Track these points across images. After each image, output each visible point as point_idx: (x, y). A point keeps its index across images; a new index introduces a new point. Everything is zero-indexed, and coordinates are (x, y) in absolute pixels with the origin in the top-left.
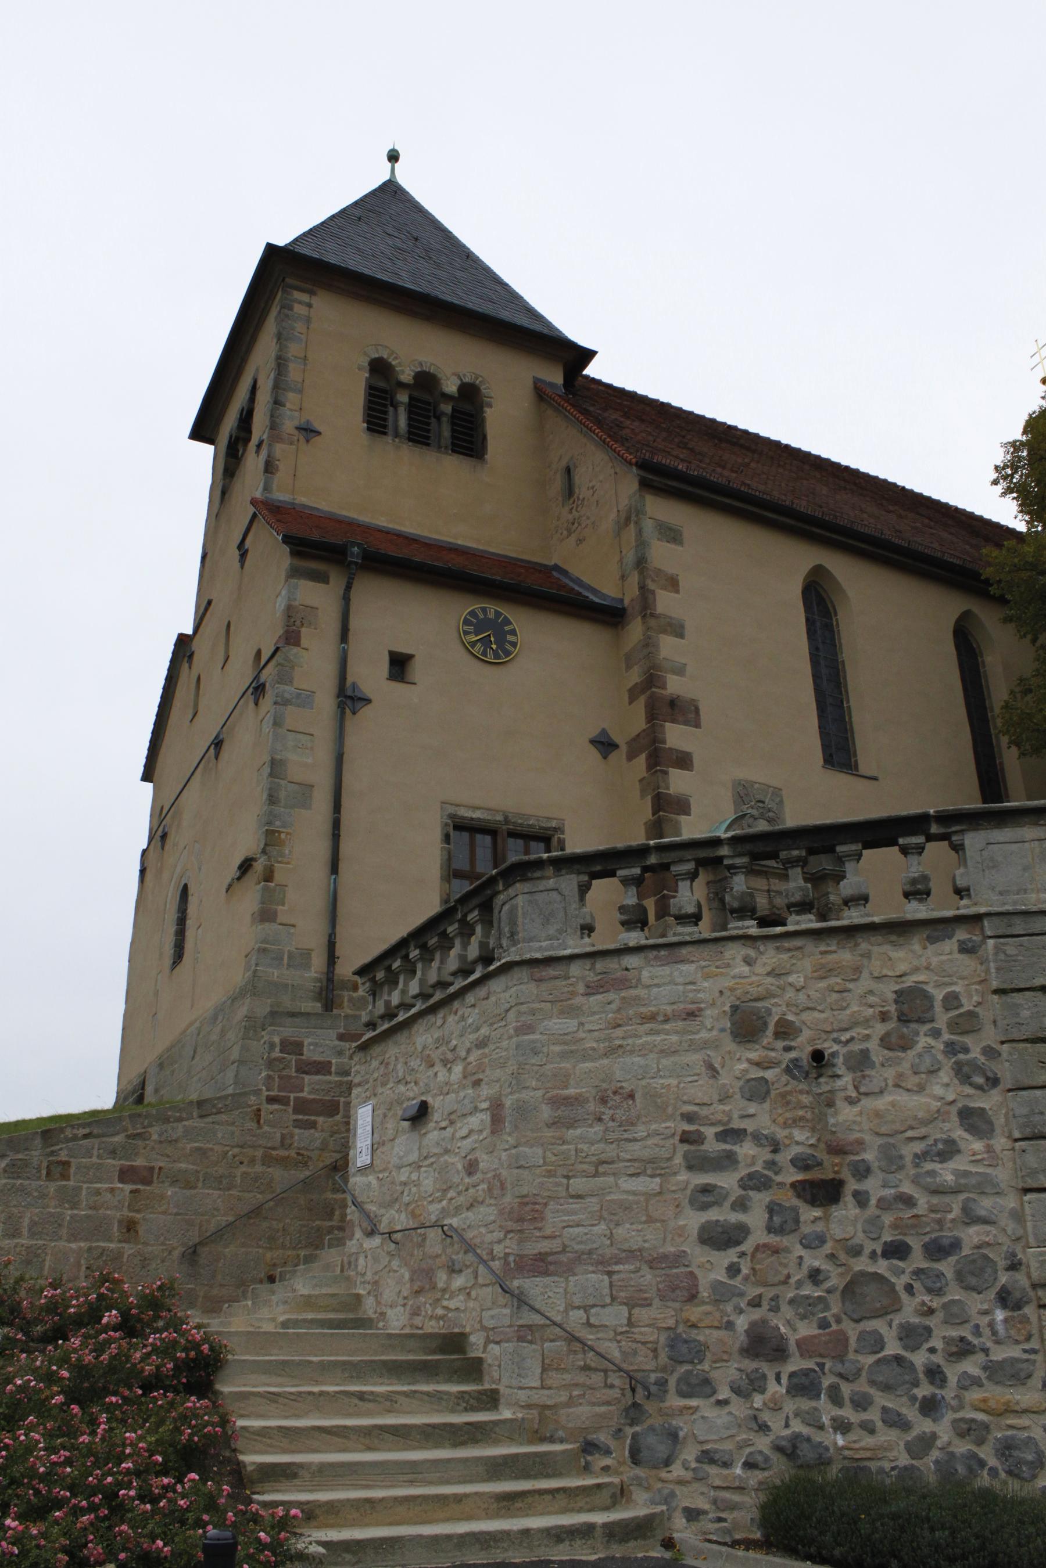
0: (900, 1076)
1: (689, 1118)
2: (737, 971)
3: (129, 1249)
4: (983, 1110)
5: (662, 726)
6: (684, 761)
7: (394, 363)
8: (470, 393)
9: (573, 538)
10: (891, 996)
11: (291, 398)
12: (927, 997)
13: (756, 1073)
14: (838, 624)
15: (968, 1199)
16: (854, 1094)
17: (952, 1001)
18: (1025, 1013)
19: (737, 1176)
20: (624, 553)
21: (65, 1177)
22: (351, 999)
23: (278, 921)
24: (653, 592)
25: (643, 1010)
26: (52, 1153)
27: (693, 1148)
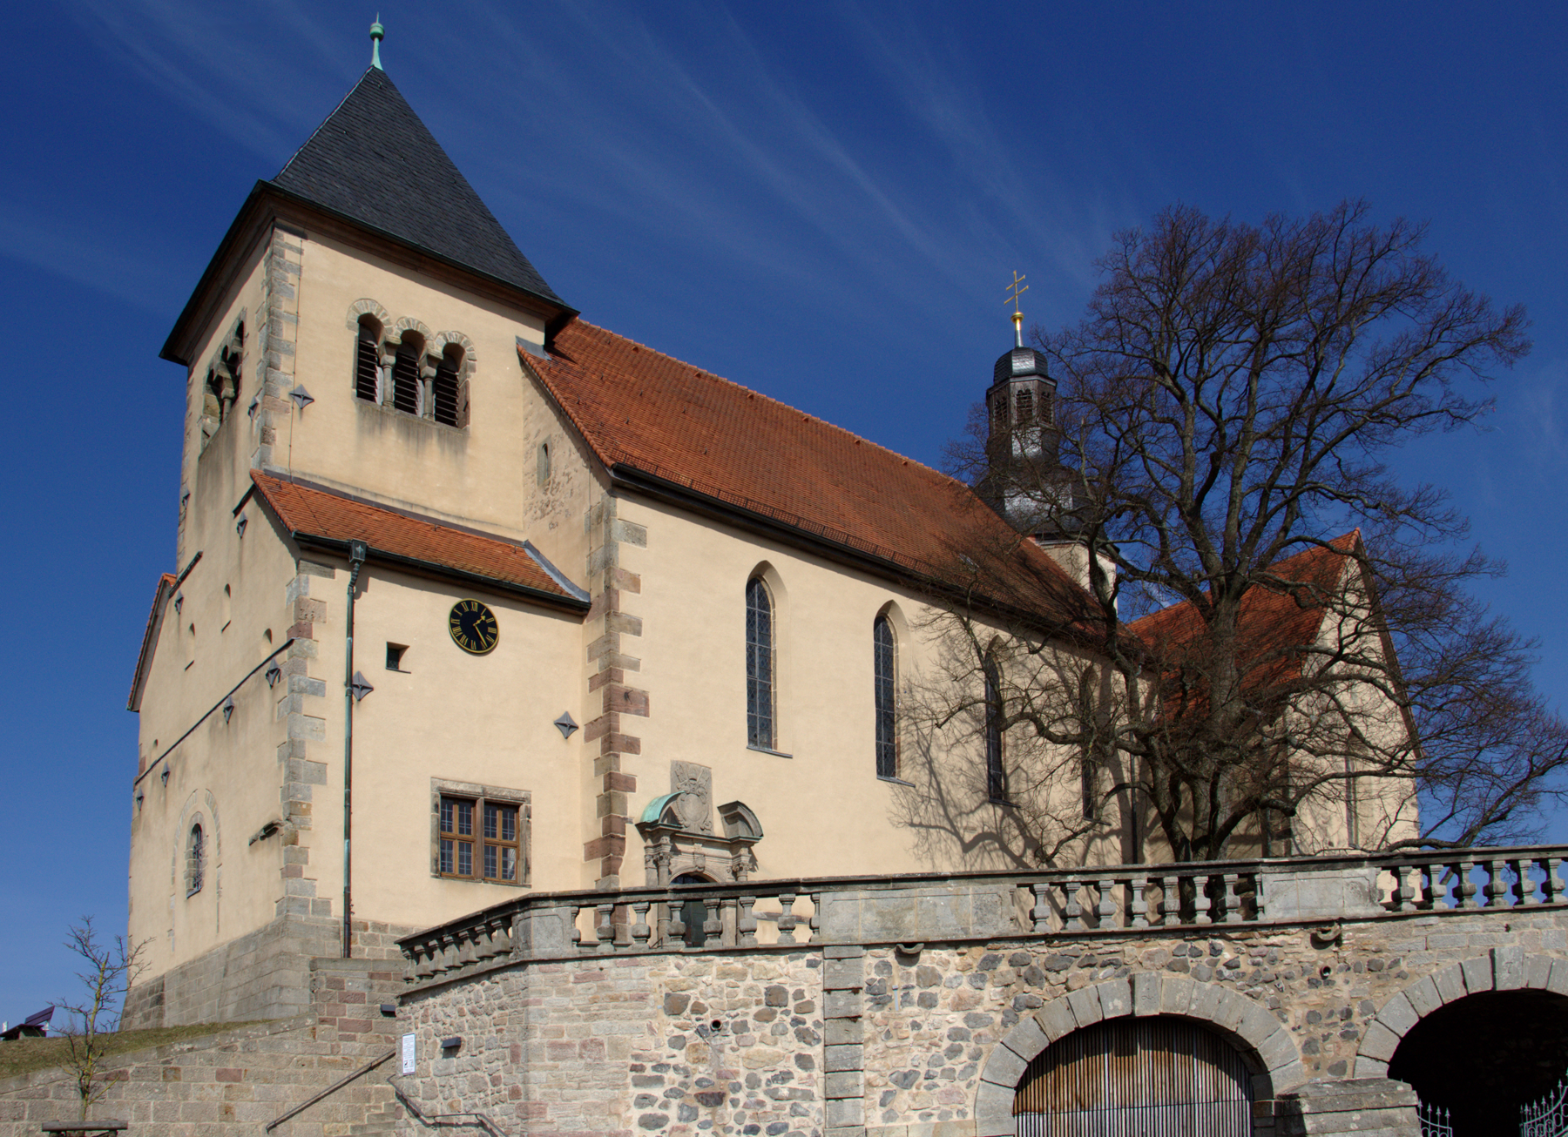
0: (763, 1036)
1: (636, 1057)
2: (671, 973)
3: (228, 1126)
4: (810, 1056)
5: (617, 716)
6: (632, 746)
7: (382, 320)
8: (454, 353)
9: (547, 520)
10: (763, 991)
11: (285, 364)
12: (785, 992)
13: (678, 1032)
14: (774, 616)
15: (795, 1104)
16: (736, 1046)
17: (799, 994)
18: (841, 1003)
19: (663, 1090)
20: (593, 549)
21: (177, 1078)
22: (362, 938)
23: (304, 876)
24: (617, 593)
25: (610, 993)
26: (168, 1062)
27: (638, 1074)
